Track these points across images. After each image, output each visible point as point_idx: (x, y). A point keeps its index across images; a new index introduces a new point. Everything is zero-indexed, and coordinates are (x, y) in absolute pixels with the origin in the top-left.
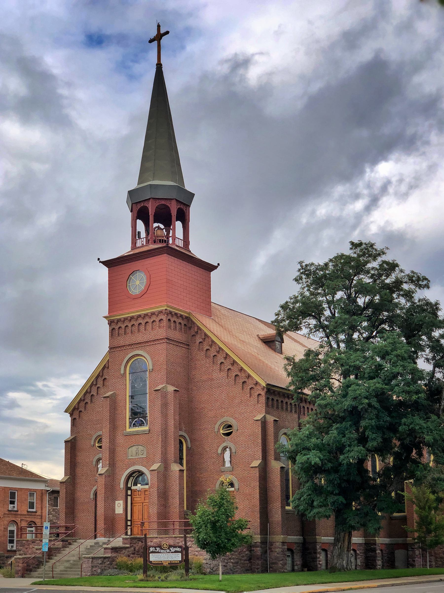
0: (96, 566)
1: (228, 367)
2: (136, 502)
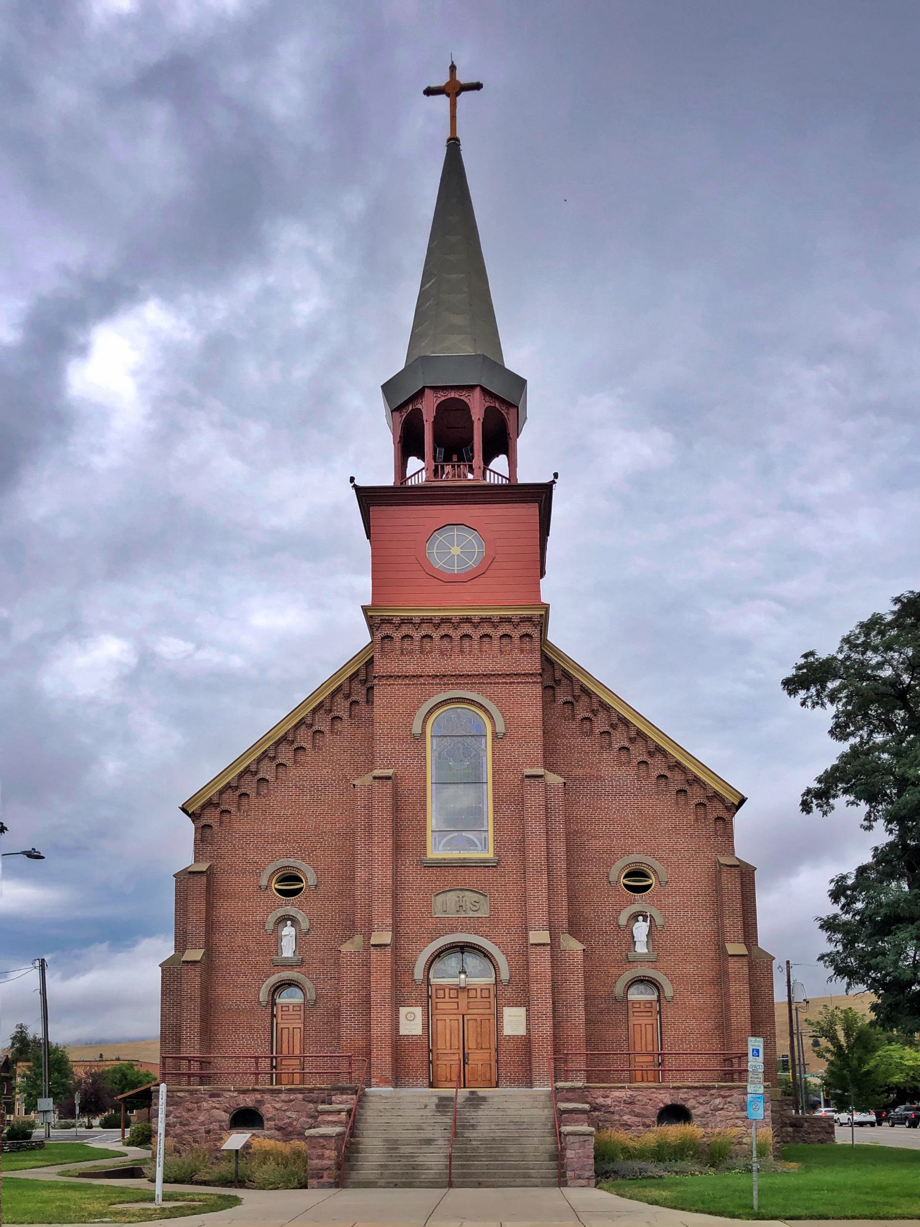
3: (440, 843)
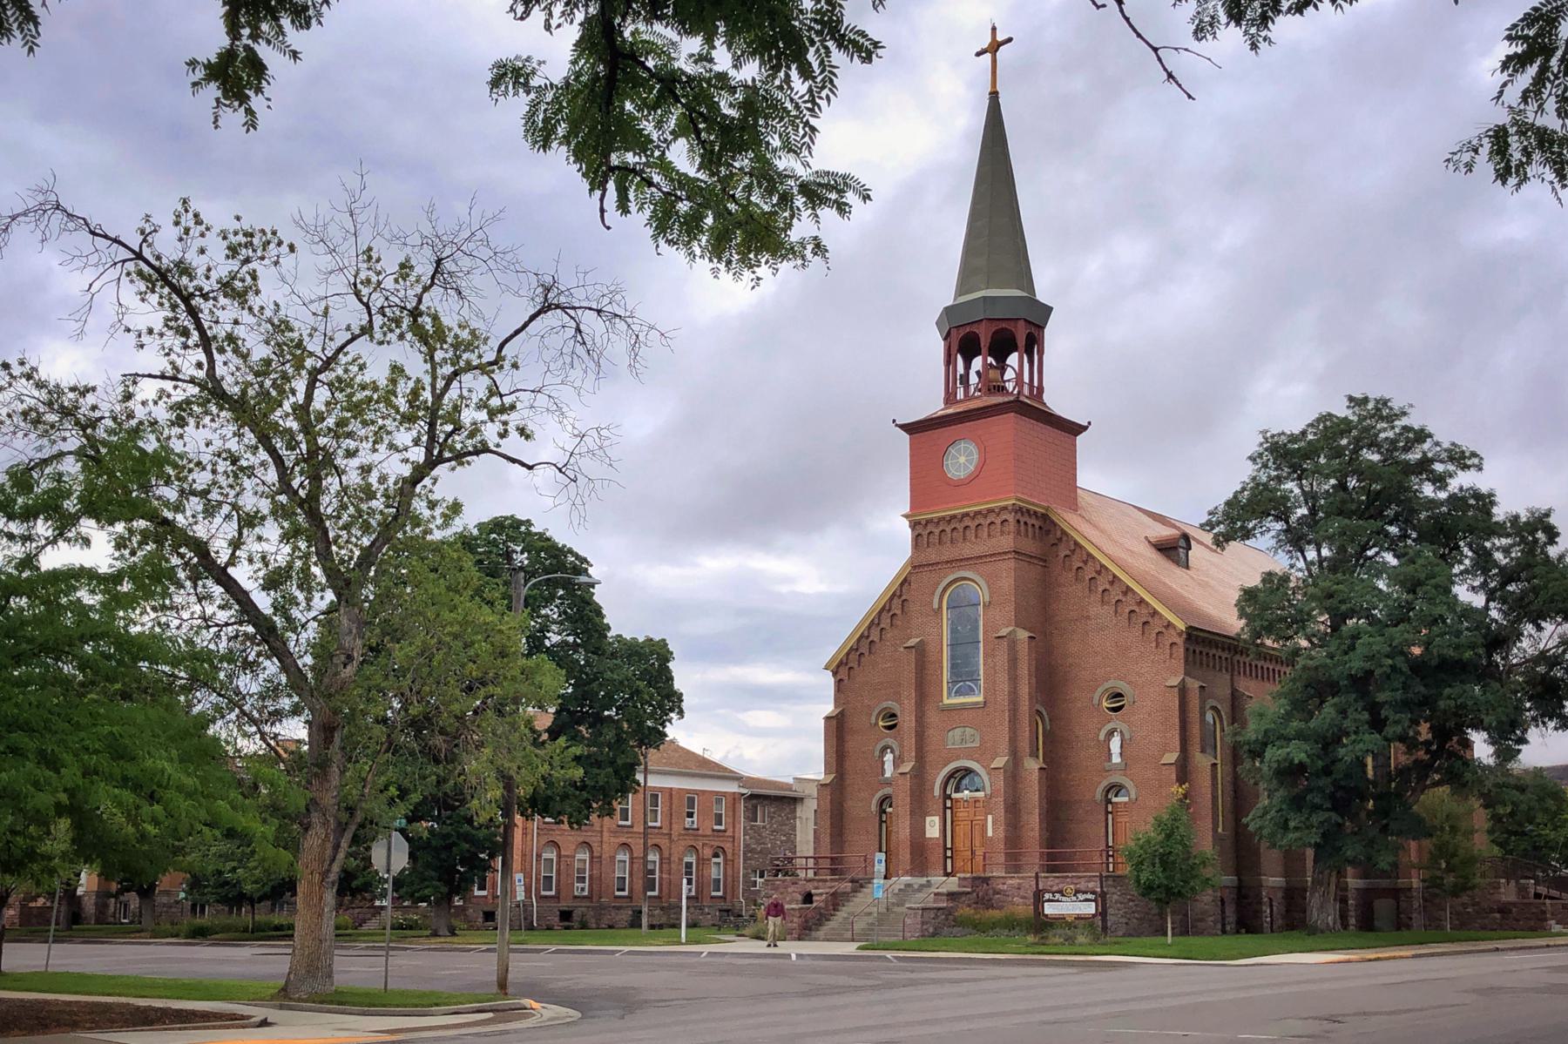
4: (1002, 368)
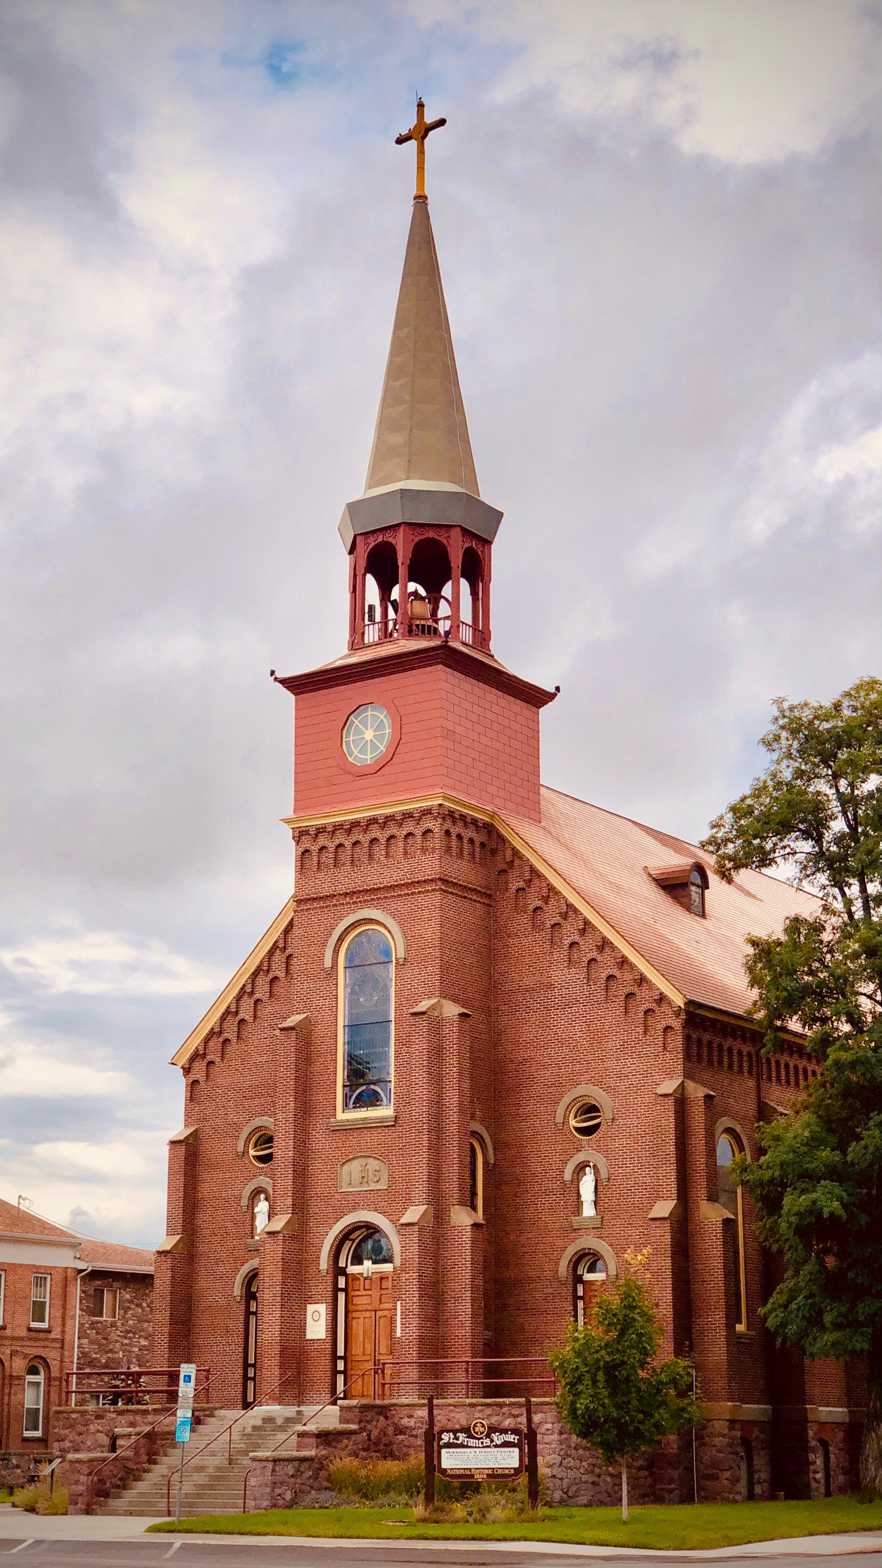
0: (282, 1483)
1: (589, 956)
2: (356, 1308)
3: (350, 1098)
4: (434, 597)
